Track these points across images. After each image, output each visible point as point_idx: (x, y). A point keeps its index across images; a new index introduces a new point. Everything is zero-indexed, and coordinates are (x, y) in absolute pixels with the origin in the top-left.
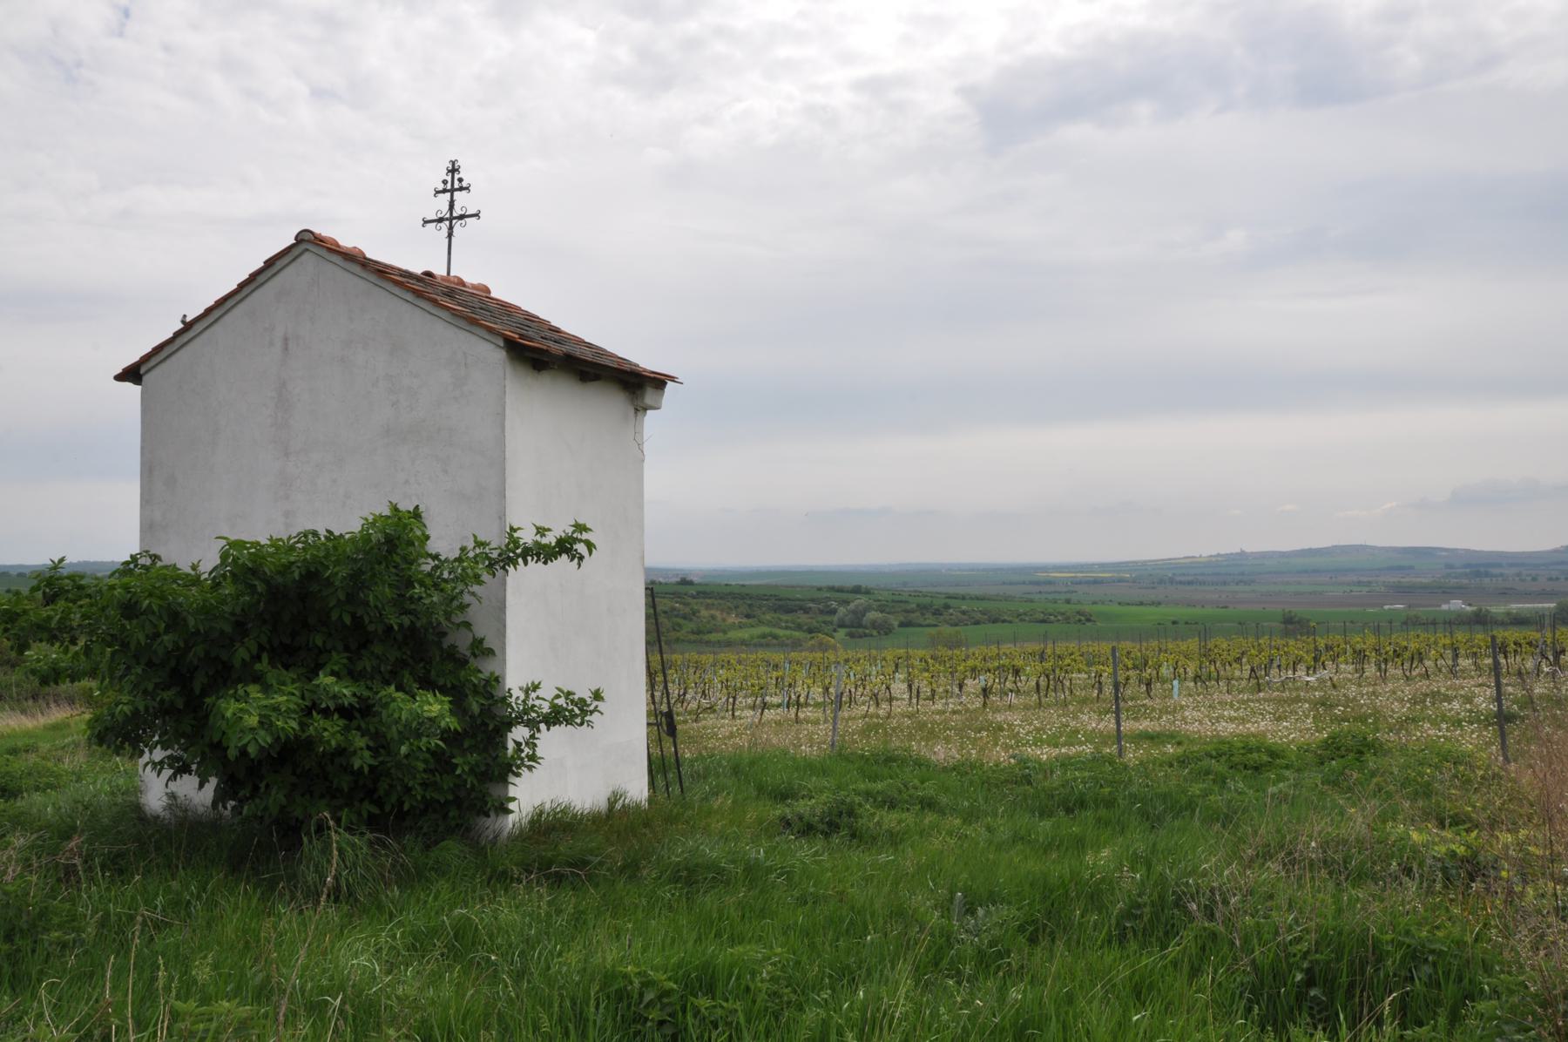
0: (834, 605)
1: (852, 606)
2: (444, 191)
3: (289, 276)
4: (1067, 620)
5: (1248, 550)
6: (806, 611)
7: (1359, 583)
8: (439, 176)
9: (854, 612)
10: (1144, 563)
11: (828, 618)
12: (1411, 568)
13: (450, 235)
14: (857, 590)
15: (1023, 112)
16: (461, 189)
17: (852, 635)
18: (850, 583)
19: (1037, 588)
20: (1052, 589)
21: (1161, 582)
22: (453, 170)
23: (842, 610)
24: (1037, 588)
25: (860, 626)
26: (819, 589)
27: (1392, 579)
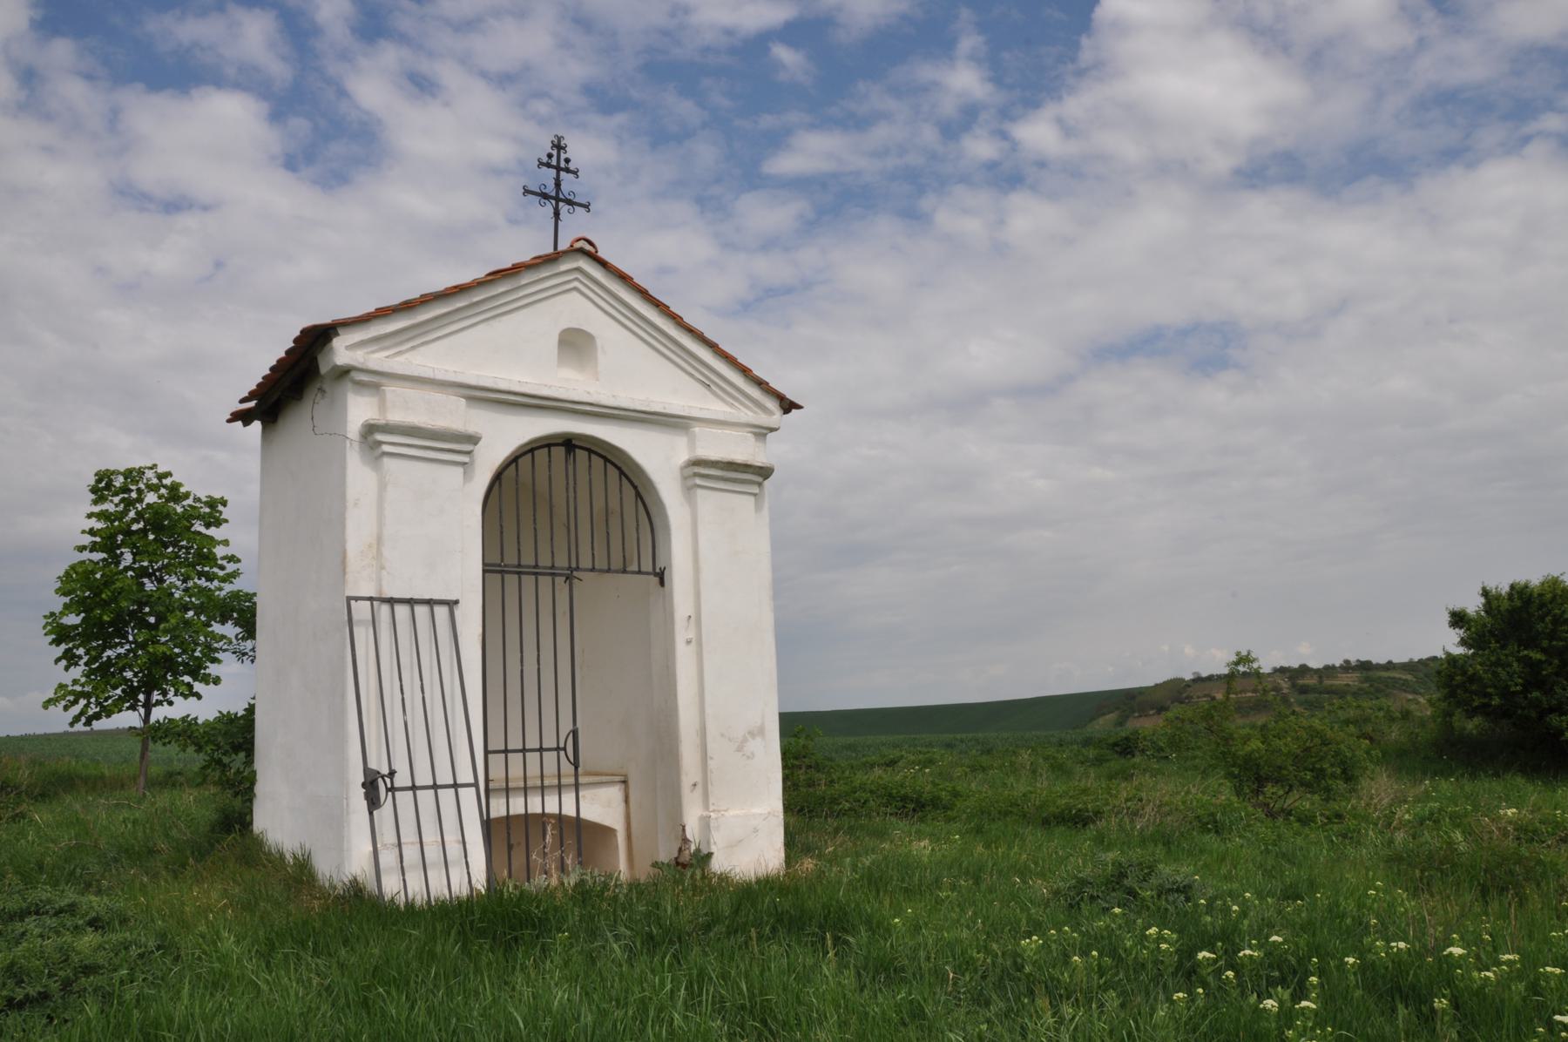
2: (548, 165)
16: (568, 170)
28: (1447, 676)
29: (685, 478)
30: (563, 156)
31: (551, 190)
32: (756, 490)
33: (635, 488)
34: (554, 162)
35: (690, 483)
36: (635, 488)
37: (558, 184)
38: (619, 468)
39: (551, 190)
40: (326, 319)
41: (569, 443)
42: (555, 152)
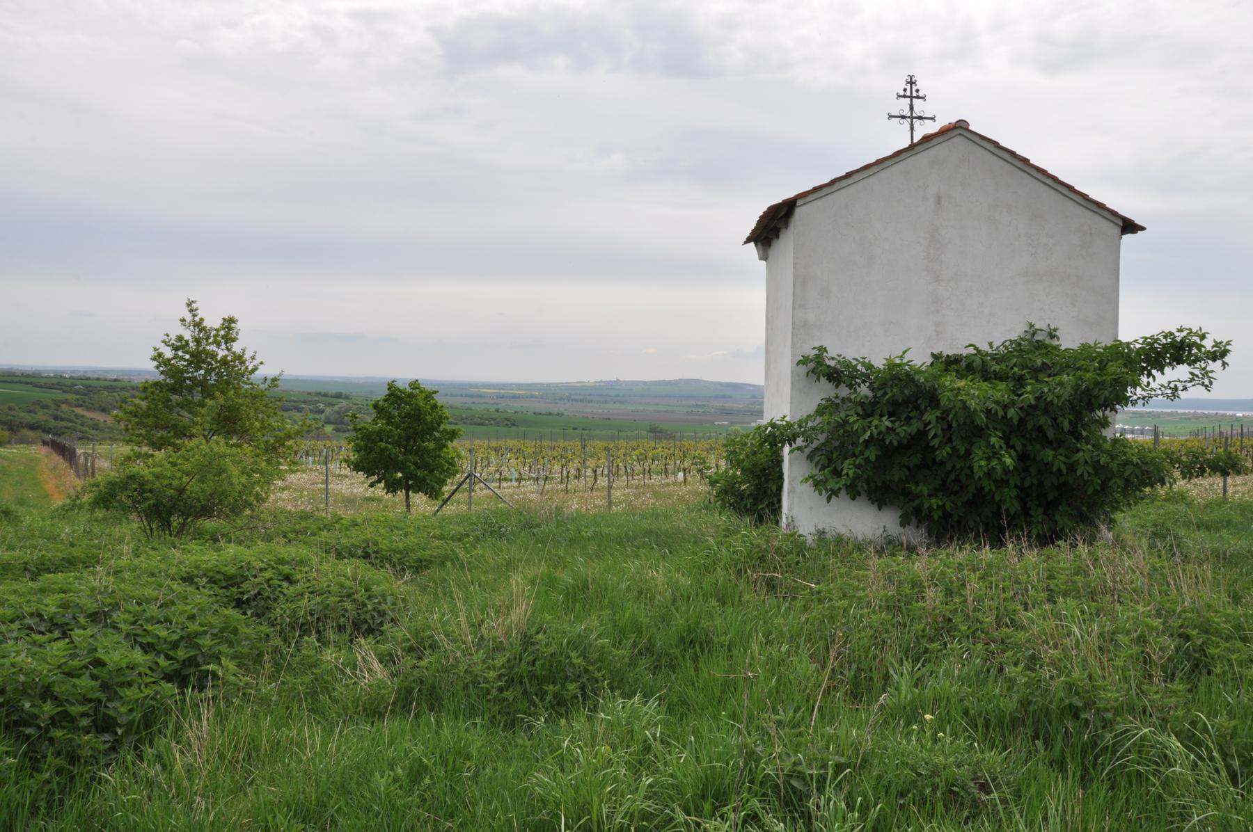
0: (322, 406)
1: (336, 408)
2: (904, 96)
3: (939, 150)
4: (498, 424)
5: (622, 379)
6: (300, 410)
7: (697, 406)
8: (900, 86)
9: (338, 413)
10: (549, 385)
11: (317, 416)
12: (730, 397)
13: (912, 129)
14: (339, 396)
15: (468, 52)
16: (918, 97)
17: (338, 430)
18: (333, 391)
19: (472, 400)
20: (482, 400)
21: (561, 399)
22: (911, 83)
23: (328, 410)
24: (472, 400)
25: (342, 423)
26: (309, 394)
27: (718, 404)
28: (149, 389)
30: (914, 88)
31: (907, 112)
34: (908, 93)
37: (912, 108)
39: (907, 112)
40: (790, 194)
42: (908, 87)
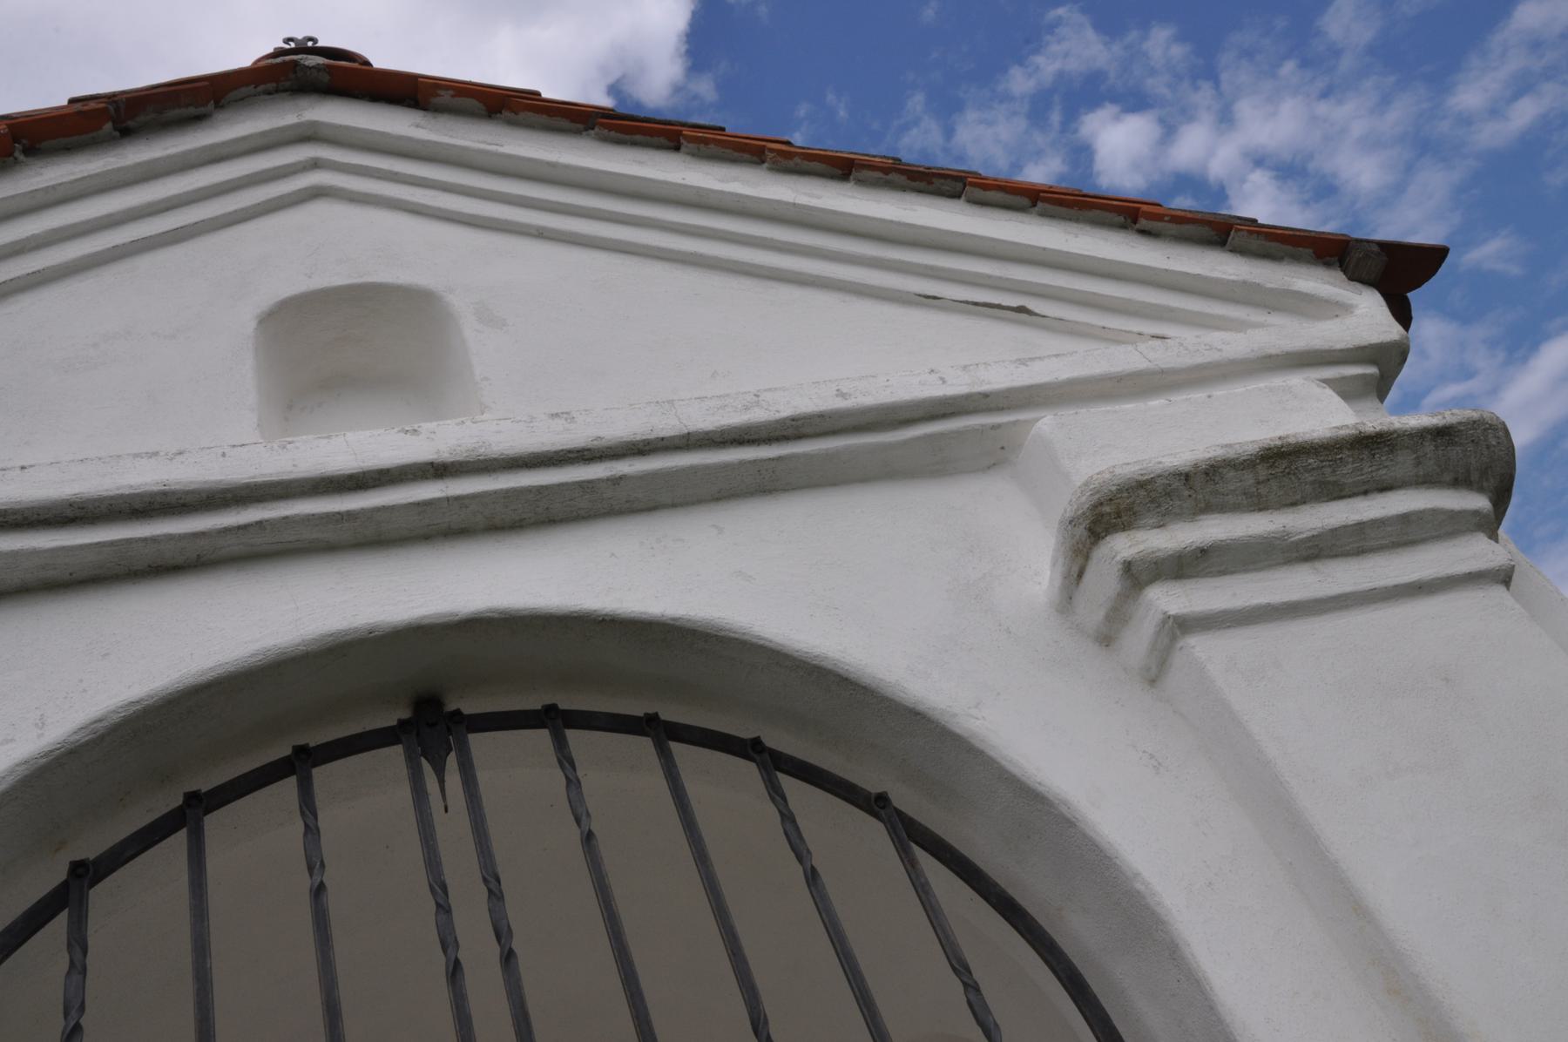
29: (1106, 639)
32: (1476, 552)
33: (877, 805)
35: (1139, 638)
36: (877, 805)
38: (751, 749)
41: (428, 699)
